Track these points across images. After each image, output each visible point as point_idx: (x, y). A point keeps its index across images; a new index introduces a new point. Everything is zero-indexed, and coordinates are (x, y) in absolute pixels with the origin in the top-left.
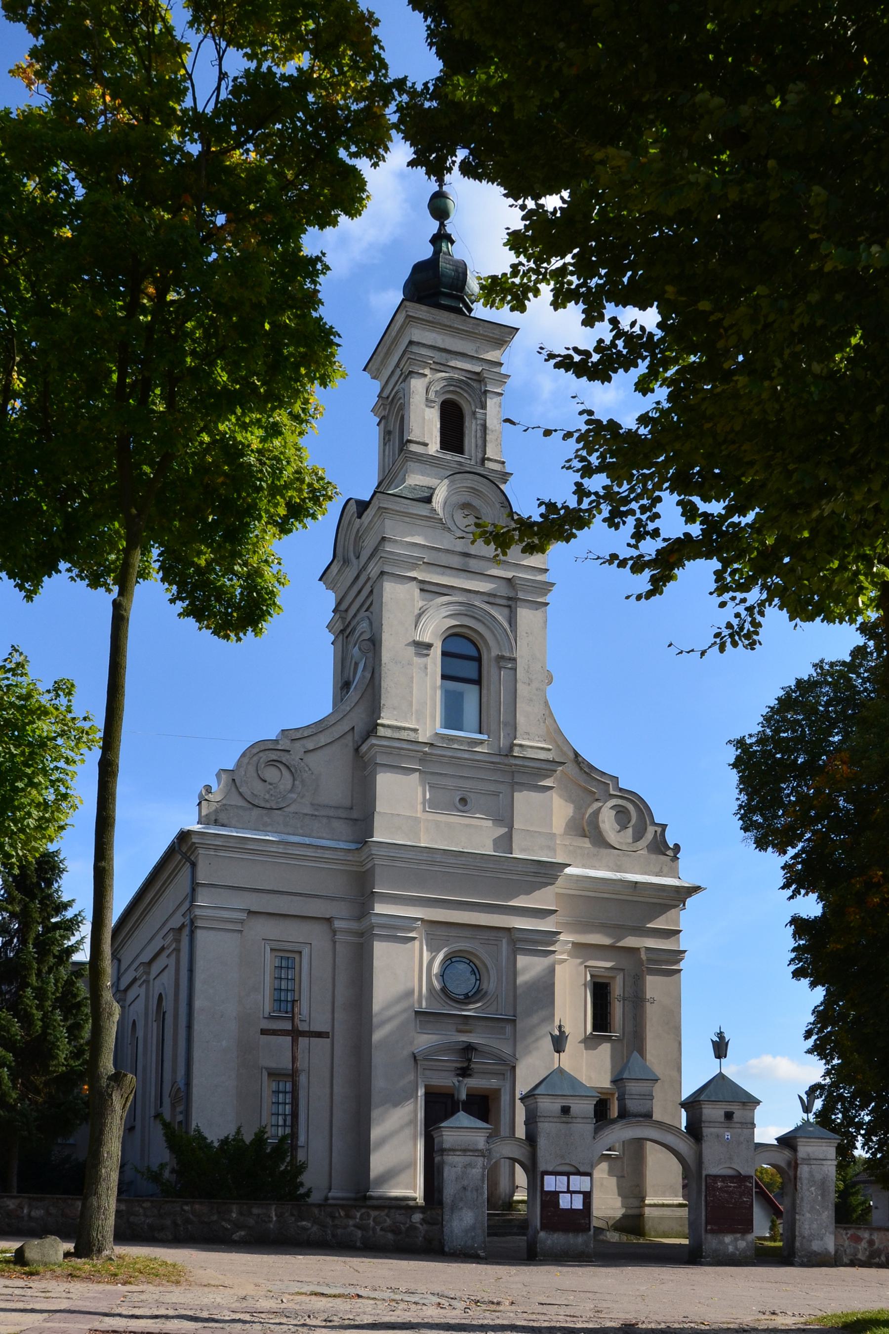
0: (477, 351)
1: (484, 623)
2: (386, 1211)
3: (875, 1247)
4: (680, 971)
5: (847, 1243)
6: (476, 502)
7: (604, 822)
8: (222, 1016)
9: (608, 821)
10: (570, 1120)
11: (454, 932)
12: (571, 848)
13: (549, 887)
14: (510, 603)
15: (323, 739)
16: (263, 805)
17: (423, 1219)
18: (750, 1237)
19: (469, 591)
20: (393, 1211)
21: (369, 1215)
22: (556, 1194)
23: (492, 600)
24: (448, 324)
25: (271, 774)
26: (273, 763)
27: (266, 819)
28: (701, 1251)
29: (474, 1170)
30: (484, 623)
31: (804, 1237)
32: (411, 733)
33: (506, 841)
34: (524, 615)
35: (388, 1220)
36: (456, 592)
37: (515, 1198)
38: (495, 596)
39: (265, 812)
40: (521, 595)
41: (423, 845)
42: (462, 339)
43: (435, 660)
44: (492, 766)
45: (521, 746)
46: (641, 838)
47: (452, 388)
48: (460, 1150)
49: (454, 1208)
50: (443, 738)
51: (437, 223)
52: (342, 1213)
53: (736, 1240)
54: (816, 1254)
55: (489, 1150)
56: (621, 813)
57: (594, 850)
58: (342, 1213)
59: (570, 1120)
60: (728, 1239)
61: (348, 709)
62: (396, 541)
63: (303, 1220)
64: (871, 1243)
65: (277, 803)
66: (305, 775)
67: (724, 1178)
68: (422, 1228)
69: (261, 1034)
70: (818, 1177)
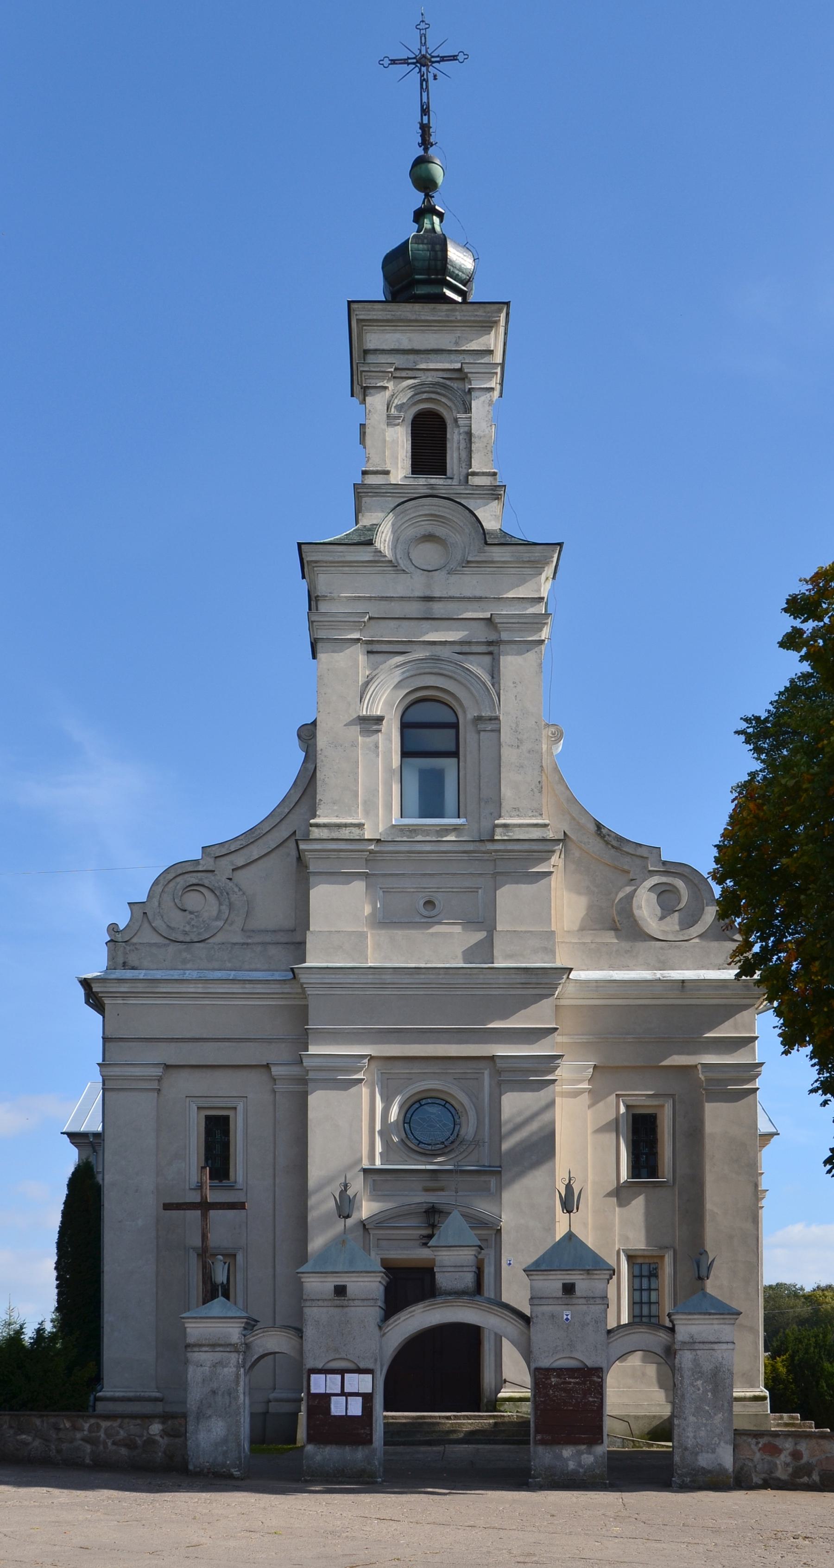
0: (456, 343)
1: (455, 680)
2: (119, 1421)
3: (804, 1460)
4: (755, 1090)
5: (758, 1455)
6: (440, 531)
7: (640, 907)
8: (137, 1191)
9: (646, 907)
10: (346, 1303)
11: (416, 1069)
12: (593, 946)
13: (545, 1000)
14: (491, 648)
15: (255, 851)
16: (181, 938)
17: (163, 1430)
18: (600, 1450)
19: (434, 643)
20: (126, 1420)
21: (99, 1427)
22: (326, 1398)
23: (466, 649)
24: (413, 318)
25: (193, 900)
26: (191, 887)
27: (184, 955)
28: (530, 1470)
29: (226, 1370)
30: (455, 680)
31: (686, 1449)
32: (353, 830)
33: (485, 949)
34: (510, 663)
35: (122, 1432)
36: (415, 647)
37: (500, 1395)
38: (469, 643)
39: (184, 946)
40: (505, 636)
41: (370, 965)
42: (436, 332)
43: (391, 737)
44: (465, 857)
45: (505, 826)
46: (696, 922)
47: (425, 396)
48: (208, 1345)
49: (200, 1416)
50: (402, 830)
51: (422, 195)
52: (68, 1425)
53: (580, 1453)
54: (704, 1471)
55: (248, 1346)
56: (664, 893)
57: (625, 945)
58: (68, 1425)
59: (346, 1303)
60: (567, 1452)
61: (287, 811)
62: (332, 599)
63: (23, 1433)
64: (796, 1455)
65: (199, 934)
66: (234, 897)
67: (560, 1372)
68: (163, 1442)
69: (164, 1209)
70: (707, 1367)
